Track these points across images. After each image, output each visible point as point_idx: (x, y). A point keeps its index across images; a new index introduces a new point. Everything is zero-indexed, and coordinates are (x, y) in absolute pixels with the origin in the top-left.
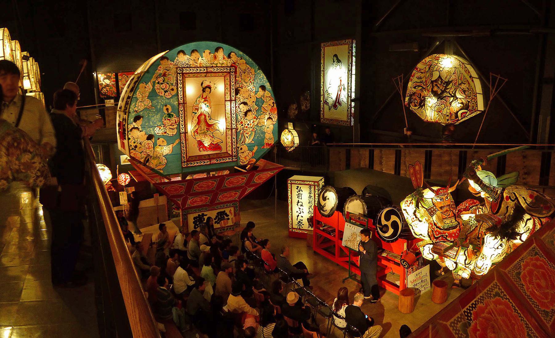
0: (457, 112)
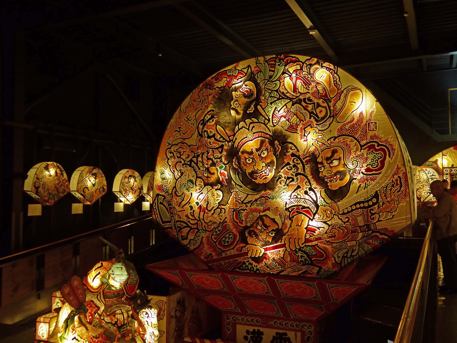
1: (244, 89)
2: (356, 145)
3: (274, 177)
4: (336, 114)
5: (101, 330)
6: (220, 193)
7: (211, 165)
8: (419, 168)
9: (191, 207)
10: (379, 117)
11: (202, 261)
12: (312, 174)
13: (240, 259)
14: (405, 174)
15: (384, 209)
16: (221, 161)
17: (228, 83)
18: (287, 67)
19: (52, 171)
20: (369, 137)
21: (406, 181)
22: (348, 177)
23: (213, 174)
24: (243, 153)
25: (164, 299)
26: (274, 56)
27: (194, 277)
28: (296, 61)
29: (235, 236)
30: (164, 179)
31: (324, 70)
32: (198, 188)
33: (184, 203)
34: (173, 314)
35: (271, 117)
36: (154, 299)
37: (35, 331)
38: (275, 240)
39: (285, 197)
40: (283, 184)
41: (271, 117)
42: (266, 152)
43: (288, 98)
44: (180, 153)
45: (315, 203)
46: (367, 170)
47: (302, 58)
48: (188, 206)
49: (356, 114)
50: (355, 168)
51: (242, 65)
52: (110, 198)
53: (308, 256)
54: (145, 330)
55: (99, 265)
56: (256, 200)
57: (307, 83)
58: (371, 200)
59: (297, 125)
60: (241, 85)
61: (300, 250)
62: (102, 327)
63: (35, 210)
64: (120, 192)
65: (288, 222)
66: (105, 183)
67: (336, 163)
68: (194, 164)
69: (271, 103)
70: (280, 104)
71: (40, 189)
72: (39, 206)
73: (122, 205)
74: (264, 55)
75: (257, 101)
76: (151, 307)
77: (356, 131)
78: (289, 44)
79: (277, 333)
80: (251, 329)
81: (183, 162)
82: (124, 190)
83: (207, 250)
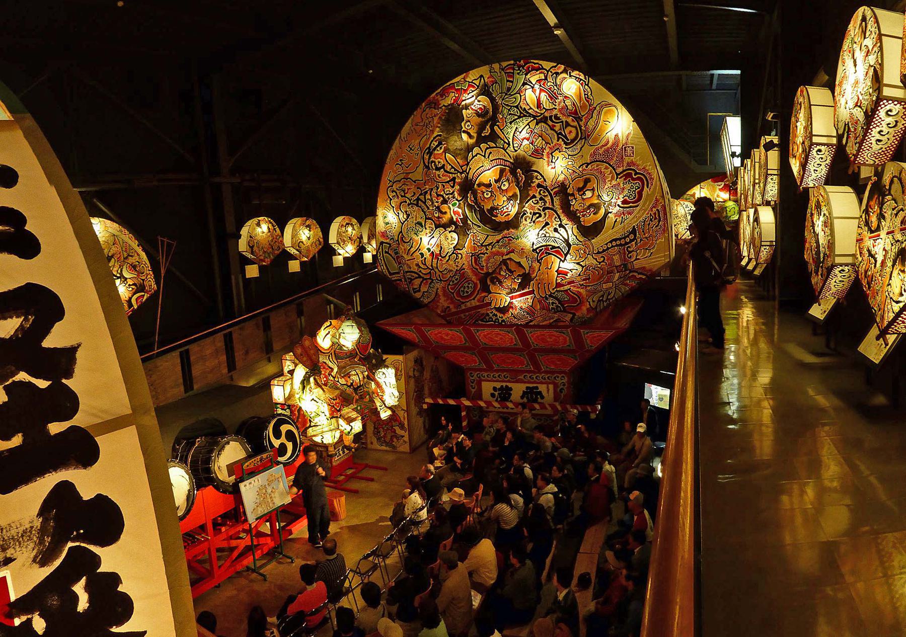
0: (130, 298)
1: (477, 105)
2: (611, 172)
3: (518, 213)
4: (589, 136)
5: (337, 392)
6: (455, 235)
7: (442, 203)
8: (677, 202)
9: (422, 255)
10: (636, 140)
11: (439, 315)
12: (562, 208)
13: (483, 311)
14: (664, 207)
15: (641, 246)
16: (454, 197)
17: (457, 99)
18: (528, 76)
19: (265, 227)
20: (625, 164)
21: (665, 214)
22: (602, 211)
23: (446, 213)
24: (479, 185)
25: (400, 358)
26: (512, 62)
27: (432, 333)
28: (539, 69)
29: (475, 284)
30: (388, 223)
31: (573, 80)
32: (428, 231)
33: (413, 250)
34: (411, 374)
35: (511, 140)
36: (390, 358)
37: (271, 394)
38: (522, 286)
39: (531, 236)
40: (529, 221)
41: (511, 140)
42: (506, 183)
43: (530, 115)
44: (404, 191)
45: (567, 241)
46: (623, 202)
47: (547, 65)
48: (418, 253)
49: (611, 136)
50: (610, 199)
51: (473, 75)
52: (327, 251)
53: (560, 304)
54: (383, 392)
55: (328, 323)
56: (498, 241)
57: (553, 97)
58: (628, 236)
59: (543, 149)
60: (473, 102)
61: (550, 296)
62: (337, 388)
63: (252, 271)
64: (338, 243)
65: (536, 265)
66: (320, 234)
67: (589, 194)
68: (421, 204)
69: (511, 123)
70: (522, 124)
71: (255, 248)
72: (255, 267)
73: (340, 258)
74: (499, 62)
75: (494, 120)
76: (387, 367)
77: (610, 156)
78: (531, 47)
79: (527, 388)
80: (498, 385)
81: (408, 201)
82: (342, 241)
83: (443, 302)
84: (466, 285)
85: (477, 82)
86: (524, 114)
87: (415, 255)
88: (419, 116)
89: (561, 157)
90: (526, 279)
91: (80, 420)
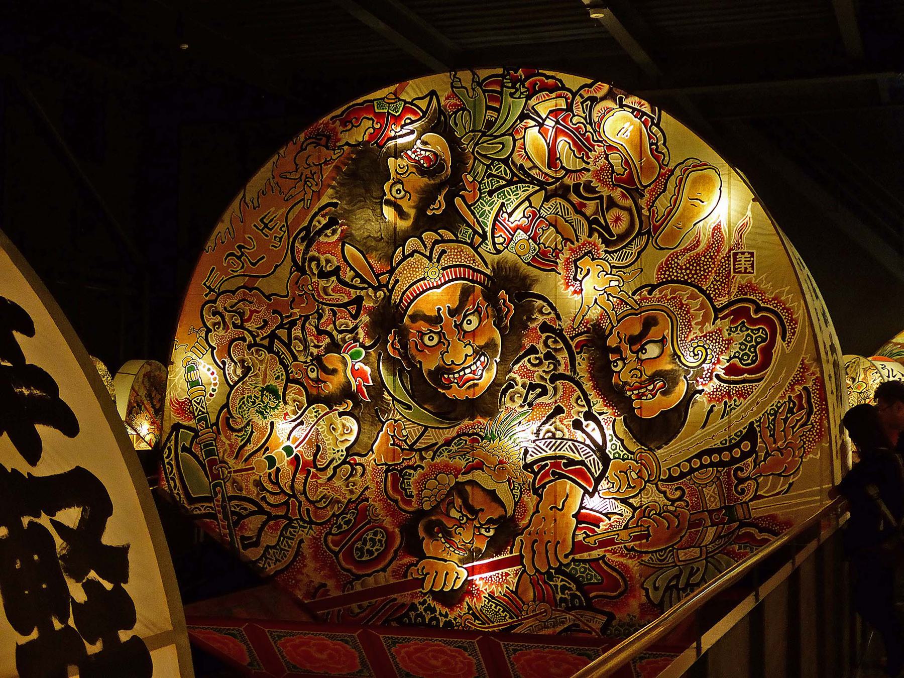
1: (420, 152)
2: (703, 306)
3: (495, 384)
4: (656, 228)
7: (328, 350)
8: (865, 362)
9: (272, 461)
11: (299, 604)
12: (593, 378)
13: (403, 598)
16: (356, 340)
18: (532, 102)
20: (734, 290)
23: (334, 372)
24: (414, 318)
26: (500, 71)
29: (390, 536)
30: (194, 383)
31: (627, 114)
32: (290, 408)
33: (250, 448)
35: (489, 229)
38: (495, 545)
39: (522, 435)
41: (489, 229)
42: (474, 319)
43: (533, 181)
44: (242, 315)
45: (601, 450)
46: (728, 371)
47: (573, 81)
48: (261, 457)
49: (705, 228)
50: (700, 362)
51: (414, 89)
56: (448, 443)
57: (582, 145)
58: (738, 445)
59: (557, 252)
61: (559, 571)
65: (530, 500)
67: (652, 350)
69: (491, 193)
70: (514, 197)
75: (454, 185)
77: (703, 271)
78: (539, 45)
81: (249, 339)
83: (312, 573)
84: (370, 535)
85: (423, 104)
86: (520, 176)
87: (254, 459)
88: (290, 158)
89: (595, 270)
90: (506, 531)
91: (139, 630)
